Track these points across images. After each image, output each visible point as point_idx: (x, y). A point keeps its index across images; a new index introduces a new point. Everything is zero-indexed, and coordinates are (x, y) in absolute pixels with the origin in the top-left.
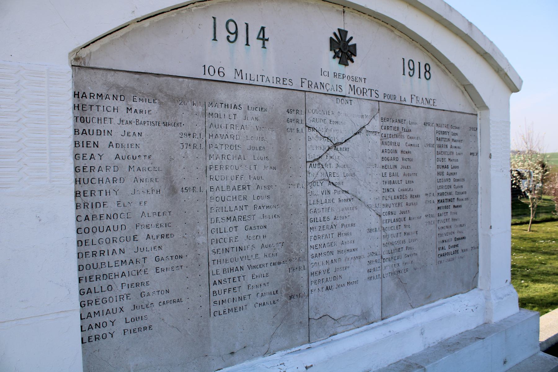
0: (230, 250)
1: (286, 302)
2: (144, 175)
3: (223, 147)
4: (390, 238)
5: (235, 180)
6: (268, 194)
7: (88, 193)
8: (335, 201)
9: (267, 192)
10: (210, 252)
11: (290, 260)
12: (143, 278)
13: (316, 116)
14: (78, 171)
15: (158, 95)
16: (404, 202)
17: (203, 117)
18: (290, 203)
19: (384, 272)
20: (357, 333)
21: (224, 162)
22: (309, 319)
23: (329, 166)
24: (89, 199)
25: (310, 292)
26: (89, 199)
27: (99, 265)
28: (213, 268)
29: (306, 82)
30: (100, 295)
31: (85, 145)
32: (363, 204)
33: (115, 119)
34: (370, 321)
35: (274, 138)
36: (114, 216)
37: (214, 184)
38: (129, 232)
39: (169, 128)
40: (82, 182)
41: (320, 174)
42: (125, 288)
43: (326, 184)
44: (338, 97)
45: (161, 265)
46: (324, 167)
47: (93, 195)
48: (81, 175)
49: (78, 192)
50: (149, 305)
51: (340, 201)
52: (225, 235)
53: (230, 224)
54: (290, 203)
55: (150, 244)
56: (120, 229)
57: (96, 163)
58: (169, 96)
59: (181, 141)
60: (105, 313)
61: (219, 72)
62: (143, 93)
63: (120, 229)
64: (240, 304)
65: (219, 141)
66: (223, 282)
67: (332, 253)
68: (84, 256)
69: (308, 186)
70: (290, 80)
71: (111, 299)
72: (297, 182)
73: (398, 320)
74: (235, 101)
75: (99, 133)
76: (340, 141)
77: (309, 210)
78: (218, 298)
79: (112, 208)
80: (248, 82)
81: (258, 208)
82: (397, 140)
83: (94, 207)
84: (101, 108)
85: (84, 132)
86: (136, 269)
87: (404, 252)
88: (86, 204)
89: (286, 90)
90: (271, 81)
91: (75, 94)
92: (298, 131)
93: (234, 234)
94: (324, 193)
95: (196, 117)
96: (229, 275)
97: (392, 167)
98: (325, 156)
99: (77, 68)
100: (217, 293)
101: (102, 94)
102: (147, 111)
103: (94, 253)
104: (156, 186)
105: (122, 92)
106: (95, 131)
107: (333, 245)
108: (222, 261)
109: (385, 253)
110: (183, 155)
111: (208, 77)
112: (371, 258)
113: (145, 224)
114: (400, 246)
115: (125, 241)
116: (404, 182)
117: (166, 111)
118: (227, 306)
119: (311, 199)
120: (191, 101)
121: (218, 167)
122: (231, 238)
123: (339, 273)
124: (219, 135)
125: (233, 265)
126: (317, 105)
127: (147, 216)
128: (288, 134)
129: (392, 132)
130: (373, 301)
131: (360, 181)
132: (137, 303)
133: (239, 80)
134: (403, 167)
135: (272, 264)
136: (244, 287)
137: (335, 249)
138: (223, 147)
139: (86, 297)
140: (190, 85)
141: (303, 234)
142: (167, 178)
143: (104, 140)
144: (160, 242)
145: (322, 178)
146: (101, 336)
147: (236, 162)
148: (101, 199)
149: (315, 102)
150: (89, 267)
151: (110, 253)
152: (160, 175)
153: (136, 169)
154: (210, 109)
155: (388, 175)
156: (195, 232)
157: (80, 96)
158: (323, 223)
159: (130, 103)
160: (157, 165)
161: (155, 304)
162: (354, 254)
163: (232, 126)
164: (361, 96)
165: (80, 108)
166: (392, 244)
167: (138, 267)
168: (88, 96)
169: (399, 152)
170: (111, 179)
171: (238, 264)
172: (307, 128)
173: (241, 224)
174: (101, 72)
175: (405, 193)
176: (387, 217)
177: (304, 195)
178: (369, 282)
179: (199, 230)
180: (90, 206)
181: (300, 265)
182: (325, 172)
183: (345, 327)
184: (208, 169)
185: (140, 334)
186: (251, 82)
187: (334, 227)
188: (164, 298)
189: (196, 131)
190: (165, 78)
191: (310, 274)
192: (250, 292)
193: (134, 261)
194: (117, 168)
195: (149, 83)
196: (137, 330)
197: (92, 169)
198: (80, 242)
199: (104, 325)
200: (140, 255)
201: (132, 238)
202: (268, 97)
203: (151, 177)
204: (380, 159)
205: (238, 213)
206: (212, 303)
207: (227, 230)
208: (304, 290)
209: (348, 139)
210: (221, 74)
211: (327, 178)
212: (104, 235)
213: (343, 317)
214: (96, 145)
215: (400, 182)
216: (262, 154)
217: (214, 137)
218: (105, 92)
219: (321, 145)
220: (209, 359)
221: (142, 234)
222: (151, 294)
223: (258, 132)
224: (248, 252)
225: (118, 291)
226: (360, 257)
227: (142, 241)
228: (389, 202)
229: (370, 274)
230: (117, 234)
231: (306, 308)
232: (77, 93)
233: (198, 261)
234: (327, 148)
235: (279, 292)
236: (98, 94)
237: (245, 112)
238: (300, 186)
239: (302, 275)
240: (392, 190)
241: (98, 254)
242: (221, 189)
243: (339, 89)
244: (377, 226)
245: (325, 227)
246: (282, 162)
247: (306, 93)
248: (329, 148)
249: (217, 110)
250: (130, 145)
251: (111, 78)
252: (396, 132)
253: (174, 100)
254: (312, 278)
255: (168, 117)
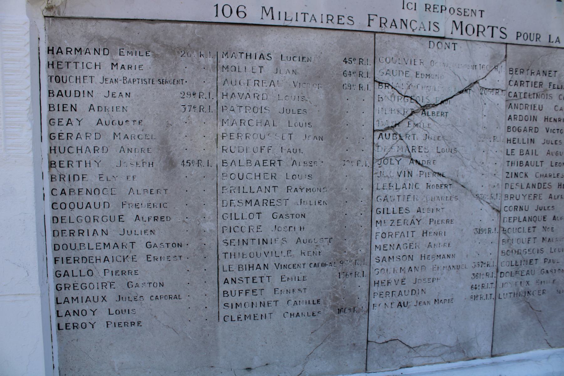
0: (250, 242)
1: (332, 317)
2: (132, 144)
3: (243, 110)
4: (515, 243)
5: (258, 154)
6: (309, 172)
7: (65, 164)
8: (420, 187)
9: (309, 170)
10: (221, 243)
11: (342, 262)
12: (129, 265)
13: (391, 66)
14: (53, 138)
15: (152, 46)
16: (545, 194)
17: (214, 71)
18: (345, 186)
19: (501, 291)
20: (443, 371)
21: (244, 129)
22: (368, 341)
23: (411, 137)
24: (66, 171)
25: (371, 307)
26: (66, 171)
27: (78, 246)
28: (225, 262)
29: (377, 20)
30: (79, 280)
31: (61, 108)
32: (469, 193)
33: (97, 78)
34: (470, 356)
35: (322, 97)
36: (96, 191)
37: (229, 157)
38: (113, 211)
39: (167, 86)
40: (57, 150)
41: (395, 148)
42: (109, 275)
43: (406, 162)
44: (431, 39)
45: (154, 252)
46: (404, 138)
47: (70, 166)
48: (56, 143)
49: (53, 163)
50: (138, 298)
51: (428, 186)
52: (242, 223)
53: (250, 209)
54: (345, 186)
55: (139, 226)
56: (102, 206)
57: (74, 129)
58: (167, 46)
59: (182, 102)
60: (84, 300)
61: (237, 12)
62: (132, 45)
63: (102, 206)
64: (262, 310)
65: (236, 101)
66: (237, 281)
67: (411, 257)
68: (60, 234)
69: (376, 165)
70: (350, 18)
71: (92, 286)
72: (357, 158)
73: (519, 361)
74: (262, 49)
75: (77, 95)
76: (433, 101)
77: (375, 196)
78: (230, 300)
79: (92, 181)
80: (282, 23)
81: (293, 190)
82: (539, 102)
83: (72, 179)
84: (80, 65)
85: (60, 94)
86: (122, 254)
87: (540, 265)
88: (62, 176)
89: (343, 32)
90: (319, 20)
91: (49, 50)
92: (360, 87)
93: (255, 222)
94: (402, 175)
95: (204, 71)
96: (246, 273)
97: (526, 141)
98: (405, 123)
99: (51, 19)
100: (229, 293)
101: (81, 49)
102: (137, 67)
103: (71, 232)
104: (149, 157)
105: (105, 44)
106: (73, 92)
107: (413, 246)
108: (237, 255)
109: (504, 264)
110: (185, 120)
111: (221, 19)
112: (478, 270)
113: (134, 203)
114: (532, 257)
115: (109, 221)
116: (546, 165)
117: (163, 65)
118: (242, 311)
119: (379, 182)
120: (197, 51)
121: (235, 136)
122: (251, 228)
123: (420, 286)
124: (236, 94)
125: (254, 261)
126: (395, 52)
127: (136, 193)
128: (344, 92)
129: (530, 90)
130: (479, 329)
131: (465, 160)
132: (123, 294)
133: (268, 20)
134: (547, 142)
135: (312, 265)
136: (269, 292)
137: (416, 253)
138: (243, 110)
139: (63, 280)
140: (196, 31)
141: (363, 229)
142: (162, 148)
143: (83, 103)
144: (152, 225)
145: (400, 153)
146: (80, 325)
147: (261, 130)
148: (79, 171)
149: (390, 47)
150: (66, 247)
151: (91, 233)
152: (153, 144)
153: (122, 136)
154: (224, 61)
155: (517, 153)
156: (199, 217)
157: (55, 51)
158: (398, 216)
159: (115, 58)
160: (150, 132)
161: (145, 298)
162: (448, 262)
163: (257, 82)
164: (474, 37)
165: (55, 66)
166: (518, 252)
167: (125, 252)
168: (64, 51)
169: (541, 121)
170: (92, 148)
171: (261, 261)
172: (377, 84)
173: (267, 210)
174: (80, 22)
175: (548, 180)
176: (512, 214)
177: (368, 175)
178: (472, 303)
179: (205, 214)
180: (66, 178)
181: (358, 270)
182: (404, 145)
183: (427, 359)
184: (220, 138)
185: (125, 328)
186: (287, 23)
187: (416, 222)
188: (157, 291)
189: (203, 90)
190: (163, 24)
191: (372, 283)
192: (277, 297)
193: (120, 245)
194: (98, 136)
195: (140, 33)
196: (123, 324)
197: (69, 136)
198: (55, 219)
199: (84, 313)
200: (126, 239)
201: (117, 218)
202: (313, 42)
203: (142, 147)
204: (503, 128)
205: (261, 196)
206: (222, 305)
207: (246, 216)
208: (362, 302)
209: (447, 100)
210: (241, 15)
211: (408, 154)
212: (84, 213)
213: (424, 345)
214: (74, 108)
215: (539, 164)
216: (301, 119)
217: (229, 97)
218: (85, 45)
219: (399, 107)
220: (216, 371)
221: (130, 214)
222: (140, 285)
223: (295, 89)
224: (277, 247)
225: (99, 277)
226: (458, 267)
227: (130, 223)
228: (517, 191)
229: (475, 292)
230: (99, 213)
231: (364, 326)
232: (51, 48)
233: (203, 252)
234: (410, 112)
235: (321, 301)
236: (76, 49)
237: (277, 63)
238: (362, 163)
239: (359, 283)
240: (523, 175)
241: (76, 233)
242: (237, 164)
243: (433, 27)
244: (493, 225)
245: (402, 221)
246: (334, 128)
247: (377, 35)
248: (413, 112)
249: (234, 62)
250: (115, 109)
251: (92, 28)
252: (537, 90)
253: (174, 51)
254: (374, 289)
255: (165, 73)
